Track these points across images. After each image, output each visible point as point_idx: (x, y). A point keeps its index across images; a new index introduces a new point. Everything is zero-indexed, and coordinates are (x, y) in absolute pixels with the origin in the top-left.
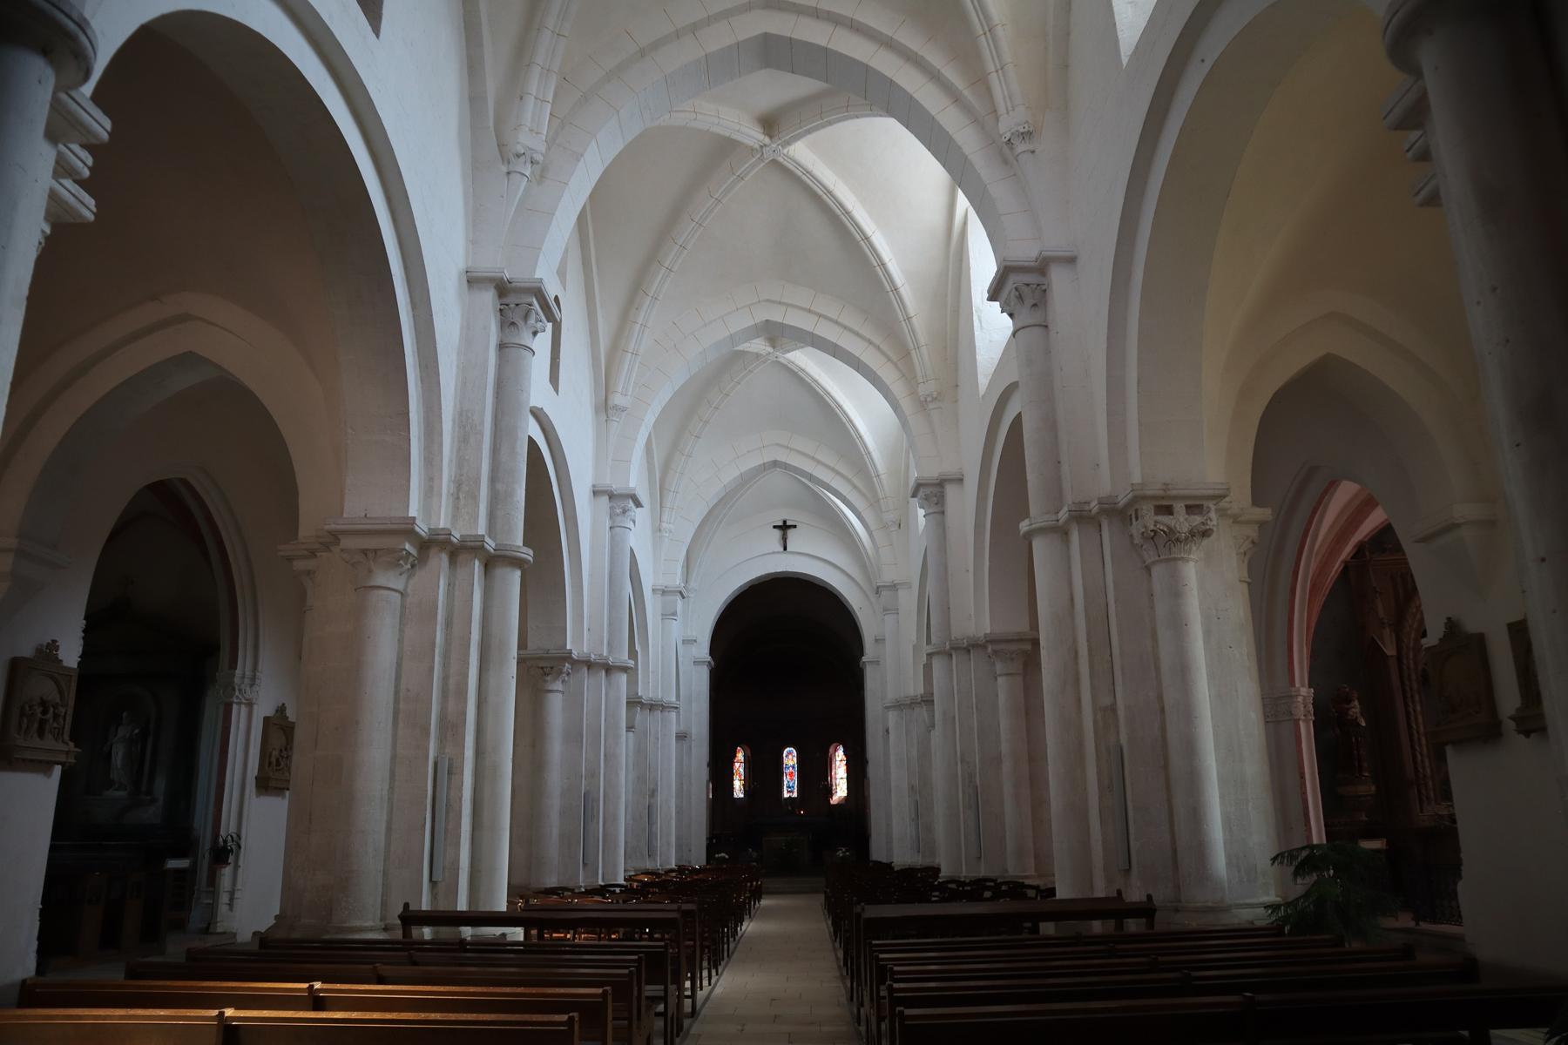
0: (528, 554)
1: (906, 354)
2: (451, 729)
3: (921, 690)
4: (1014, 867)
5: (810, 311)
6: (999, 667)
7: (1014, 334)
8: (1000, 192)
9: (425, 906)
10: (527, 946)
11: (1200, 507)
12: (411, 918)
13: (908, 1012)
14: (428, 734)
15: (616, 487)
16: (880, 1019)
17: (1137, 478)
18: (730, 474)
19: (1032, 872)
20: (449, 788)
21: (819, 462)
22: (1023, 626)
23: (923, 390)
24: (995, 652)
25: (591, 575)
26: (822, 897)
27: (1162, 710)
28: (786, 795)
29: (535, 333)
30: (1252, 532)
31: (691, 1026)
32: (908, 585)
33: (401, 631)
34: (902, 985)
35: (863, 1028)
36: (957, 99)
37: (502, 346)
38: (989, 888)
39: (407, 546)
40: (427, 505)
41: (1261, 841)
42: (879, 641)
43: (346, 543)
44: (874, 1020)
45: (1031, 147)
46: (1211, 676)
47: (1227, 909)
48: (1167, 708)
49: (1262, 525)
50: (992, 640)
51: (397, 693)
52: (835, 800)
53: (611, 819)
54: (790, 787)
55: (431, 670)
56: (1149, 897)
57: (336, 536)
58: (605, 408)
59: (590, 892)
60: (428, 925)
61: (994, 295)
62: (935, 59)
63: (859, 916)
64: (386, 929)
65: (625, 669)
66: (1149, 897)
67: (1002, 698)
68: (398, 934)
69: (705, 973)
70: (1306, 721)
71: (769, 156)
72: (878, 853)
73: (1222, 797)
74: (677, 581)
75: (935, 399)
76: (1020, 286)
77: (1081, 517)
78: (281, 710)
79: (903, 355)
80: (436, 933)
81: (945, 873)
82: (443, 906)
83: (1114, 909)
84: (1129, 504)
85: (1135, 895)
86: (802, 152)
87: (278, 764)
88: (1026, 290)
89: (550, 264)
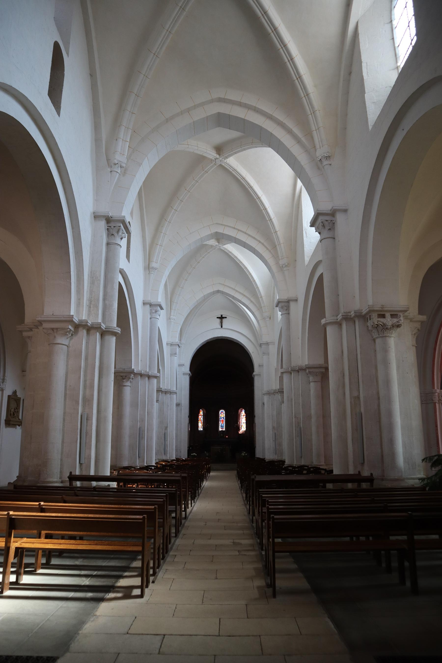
0: (118, 330)
1: (274, 247)
2: (87, 401)
3: (278, 387)
4: (316, 460)
5: (234, 228)
6: (311, 378)
7: (321, 241)
8: (316, 181)
9: (78, 473)
10: (118, 490)
11: (397, 315)
12: (72, 478)
13: (276, 517)
14: (78, 404)
15: (153, 301)
16: (263, 521)
17: (370, 303)
18: (200, 296)
19: (323, 463)
20: (87, 426)
21: (237, 291)
22: (321, 361)
23: (281, 262)
24: (309, 372)
25: (142, 338)
26: (236, 472)
27: (379, 398)
28: (220, 429)
29: (122, 239)
30: (418, 325)
31: (185, 523)
32: (273, 343)
33: (67, 362)
34: (272, 507)
35: (254, 525)
36: (299, 141)
37: (108, 244)
38: (305, 470)
39: (70, 327)
40: (78, 310)
41: (418, 453)
42: (261, 366)
43: (45, 325)
44: (260, 521)
45: (330, 163)
46: (399, 384)
47: (403, 480)
48: (381, 397)
49: (422, 322)
50: (308, 367)
51: (66, 387)
52: (241, 432)
53: (150, 439)
54: (222, 426)
55: (80, 378)
56: (372, 474)
57: (40, 323)
58: (148, 268)
59: (142, 468)
60: (79, 480)
61: (313, 224)
62: (290, 124)
63: (253, 480)
64: (62, 482)
65: (156, 377)
66: (372, 474)
67: (312, 392)
68: (68, 484)
69: (190, 502)
70: (439, 403)
71: (218, 163)
72: (259, 454)
73: (402, 434)
74: (177, 340)
75: (286, 266)
76: (324, 221)
77: (347, 318)
78: (15, 392)
79: (273, 247)
80: (82, 484)
81: (287, 463)
82: (84, 473)
83: (357, 479)
84: (367, 314)
85: (366, 473)
86: (233, 161)
87: (14, 414)
88: (326, 222)
89: (128, 210)
